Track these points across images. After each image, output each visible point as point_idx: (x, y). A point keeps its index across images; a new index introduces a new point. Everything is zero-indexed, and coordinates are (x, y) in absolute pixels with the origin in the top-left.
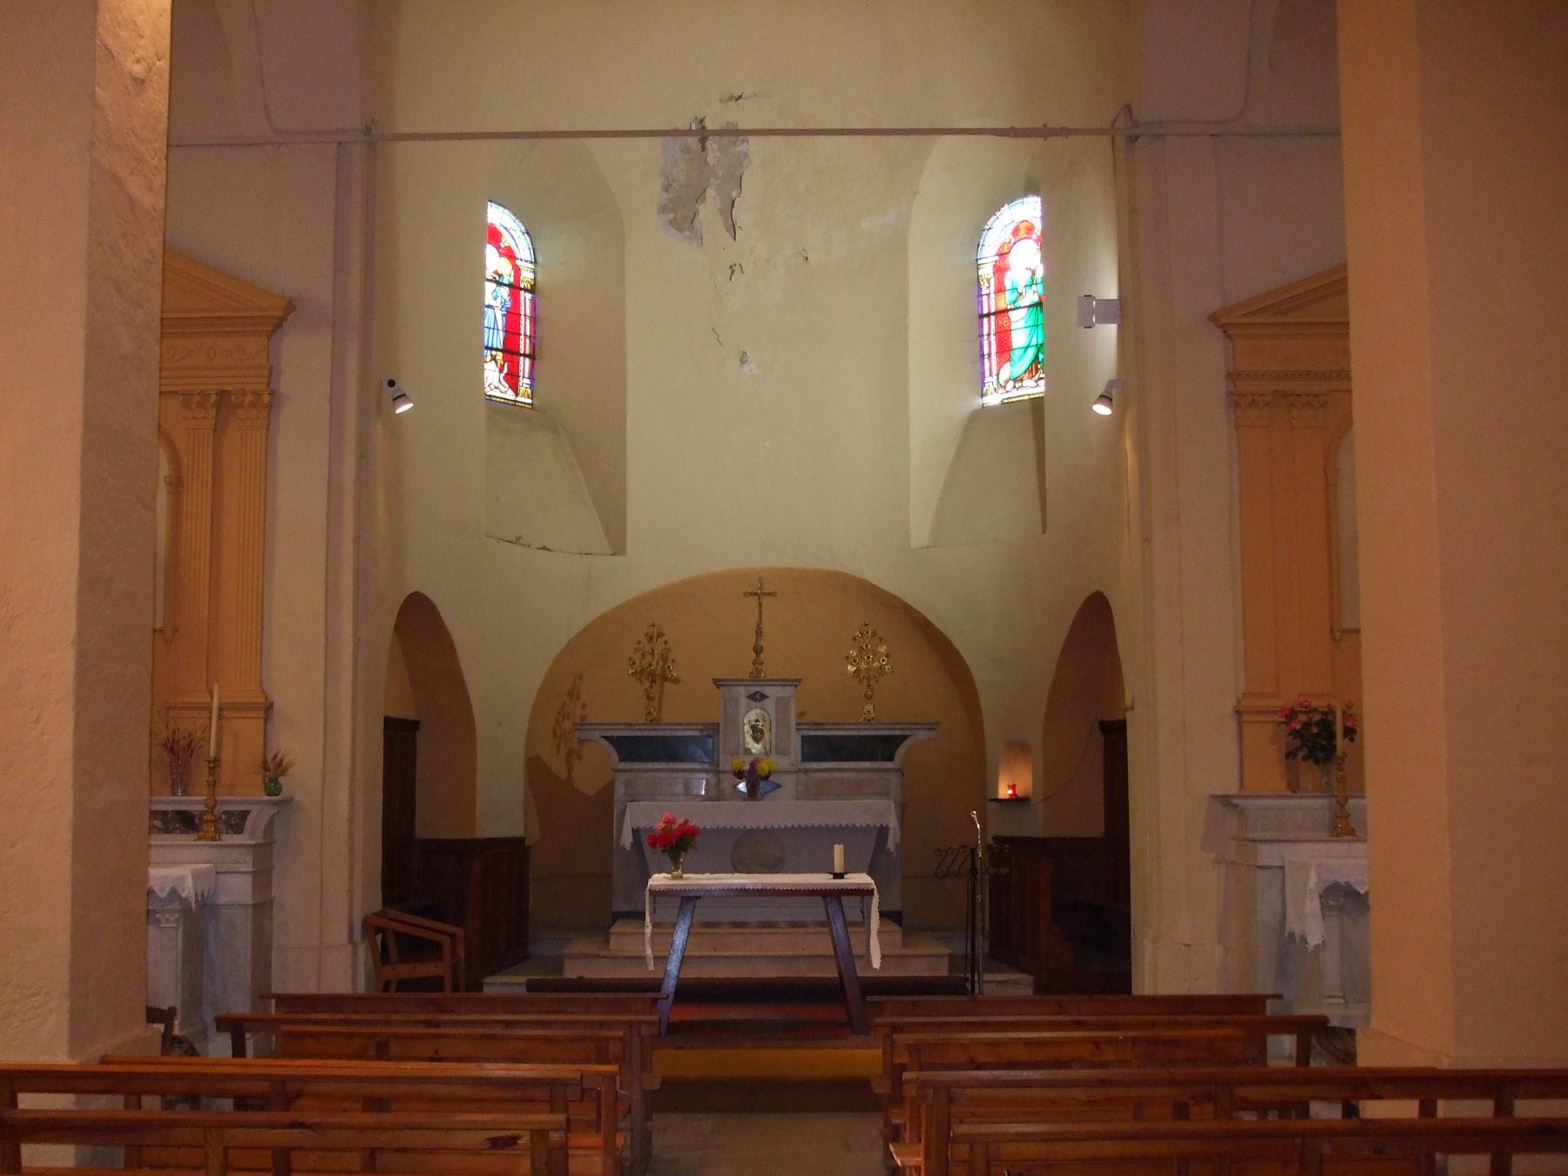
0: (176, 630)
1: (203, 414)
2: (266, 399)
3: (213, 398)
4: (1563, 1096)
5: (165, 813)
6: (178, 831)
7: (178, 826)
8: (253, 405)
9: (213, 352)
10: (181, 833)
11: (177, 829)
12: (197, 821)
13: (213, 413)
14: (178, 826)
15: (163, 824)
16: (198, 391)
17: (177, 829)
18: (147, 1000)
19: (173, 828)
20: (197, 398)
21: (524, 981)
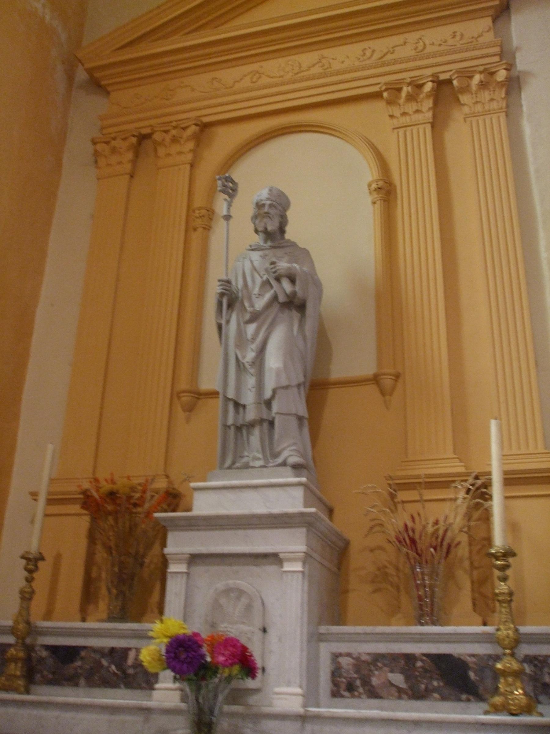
0: (397, 376)
1: (415, 108)
2: (501, 75)
3: (429, 86)
4: (1, 626)
5: (410, 658)
6: (436, 695)
7: (435, 683)
8: (483, 85)
9: (421, 44)
10: (444, 698)
11: (435, 690)
12: (472, 675)
13: (429, 103)
14: (435, 683)
15: (407, 679)
16: (408, 80)
17: (435, 690)
18: (228, 225)
19: (427, 689)
20: (406, 90)
21: (231, 650)
